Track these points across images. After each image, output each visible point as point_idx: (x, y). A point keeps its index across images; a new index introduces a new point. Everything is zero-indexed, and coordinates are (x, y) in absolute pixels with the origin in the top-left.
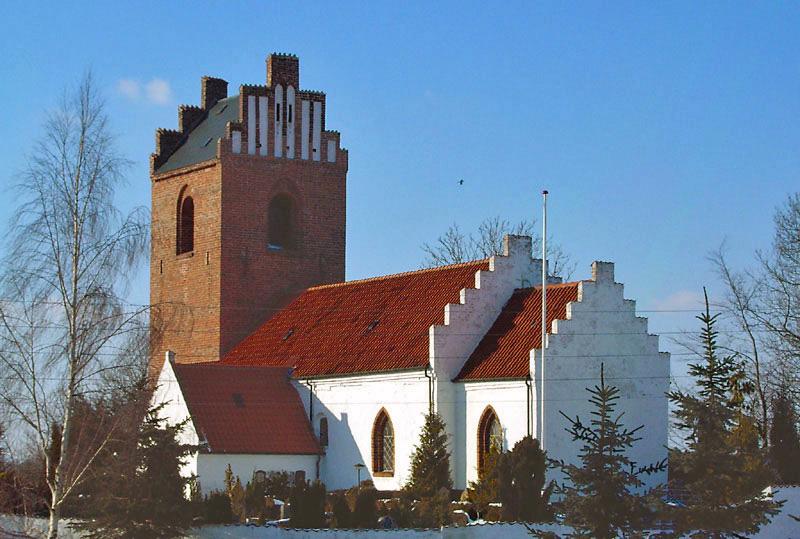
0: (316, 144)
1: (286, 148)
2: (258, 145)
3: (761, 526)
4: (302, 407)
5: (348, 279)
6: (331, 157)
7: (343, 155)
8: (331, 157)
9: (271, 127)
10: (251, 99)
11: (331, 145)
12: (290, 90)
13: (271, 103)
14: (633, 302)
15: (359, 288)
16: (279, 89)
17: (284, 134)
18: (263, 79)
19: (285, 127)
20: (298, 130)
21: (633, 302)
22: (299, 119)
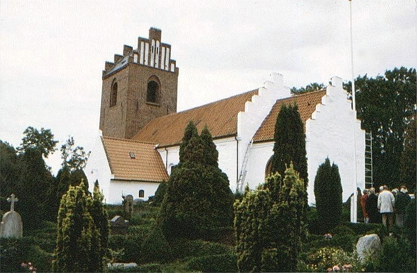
0: (167, 64)
1: (155, 64)
2: (144, 61)
3: (200, 130)
4: (162, 162)
5: (178, 110)
6: (173, 70)
7: (177, 69)
8: (173, 70)
9: (149, 54)
10: (142, 43)
11: (173, 65)
12: (158, 42)
13: (150, 45)
14: (116, 56)
15: (179, 113)
16: (153, 42)
17: (155, 59)
18: (147, 36)
19: (155, 56)
20: (160, 57)
21: (116, 56)
22: (160, 53)
